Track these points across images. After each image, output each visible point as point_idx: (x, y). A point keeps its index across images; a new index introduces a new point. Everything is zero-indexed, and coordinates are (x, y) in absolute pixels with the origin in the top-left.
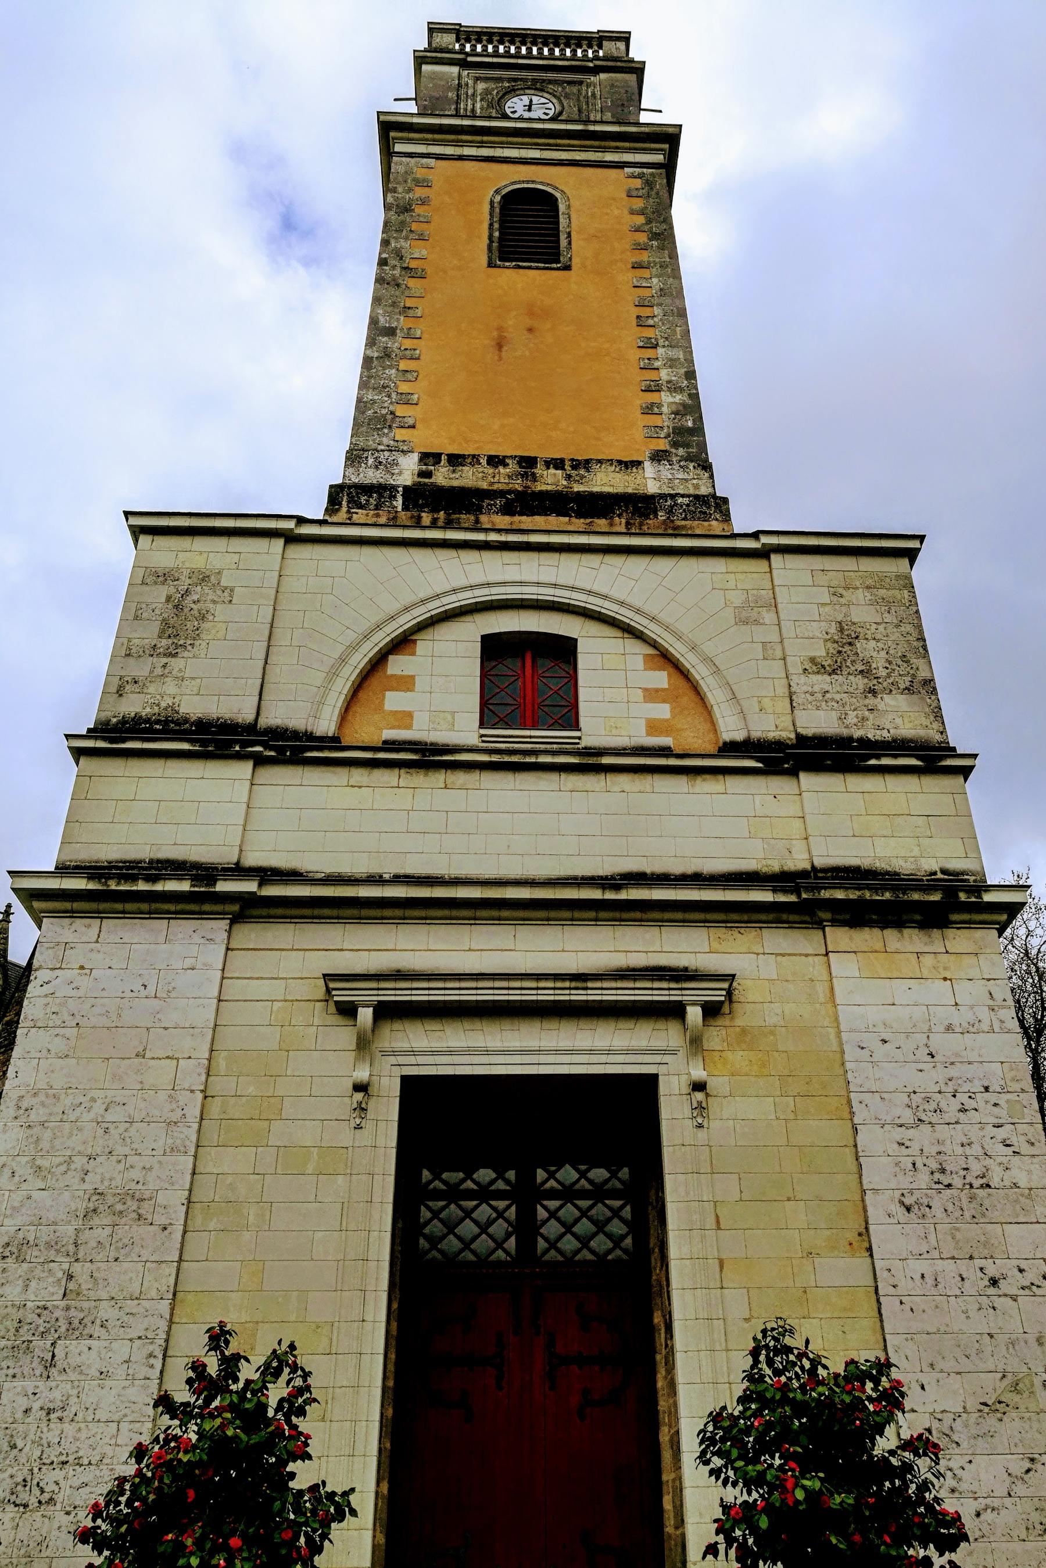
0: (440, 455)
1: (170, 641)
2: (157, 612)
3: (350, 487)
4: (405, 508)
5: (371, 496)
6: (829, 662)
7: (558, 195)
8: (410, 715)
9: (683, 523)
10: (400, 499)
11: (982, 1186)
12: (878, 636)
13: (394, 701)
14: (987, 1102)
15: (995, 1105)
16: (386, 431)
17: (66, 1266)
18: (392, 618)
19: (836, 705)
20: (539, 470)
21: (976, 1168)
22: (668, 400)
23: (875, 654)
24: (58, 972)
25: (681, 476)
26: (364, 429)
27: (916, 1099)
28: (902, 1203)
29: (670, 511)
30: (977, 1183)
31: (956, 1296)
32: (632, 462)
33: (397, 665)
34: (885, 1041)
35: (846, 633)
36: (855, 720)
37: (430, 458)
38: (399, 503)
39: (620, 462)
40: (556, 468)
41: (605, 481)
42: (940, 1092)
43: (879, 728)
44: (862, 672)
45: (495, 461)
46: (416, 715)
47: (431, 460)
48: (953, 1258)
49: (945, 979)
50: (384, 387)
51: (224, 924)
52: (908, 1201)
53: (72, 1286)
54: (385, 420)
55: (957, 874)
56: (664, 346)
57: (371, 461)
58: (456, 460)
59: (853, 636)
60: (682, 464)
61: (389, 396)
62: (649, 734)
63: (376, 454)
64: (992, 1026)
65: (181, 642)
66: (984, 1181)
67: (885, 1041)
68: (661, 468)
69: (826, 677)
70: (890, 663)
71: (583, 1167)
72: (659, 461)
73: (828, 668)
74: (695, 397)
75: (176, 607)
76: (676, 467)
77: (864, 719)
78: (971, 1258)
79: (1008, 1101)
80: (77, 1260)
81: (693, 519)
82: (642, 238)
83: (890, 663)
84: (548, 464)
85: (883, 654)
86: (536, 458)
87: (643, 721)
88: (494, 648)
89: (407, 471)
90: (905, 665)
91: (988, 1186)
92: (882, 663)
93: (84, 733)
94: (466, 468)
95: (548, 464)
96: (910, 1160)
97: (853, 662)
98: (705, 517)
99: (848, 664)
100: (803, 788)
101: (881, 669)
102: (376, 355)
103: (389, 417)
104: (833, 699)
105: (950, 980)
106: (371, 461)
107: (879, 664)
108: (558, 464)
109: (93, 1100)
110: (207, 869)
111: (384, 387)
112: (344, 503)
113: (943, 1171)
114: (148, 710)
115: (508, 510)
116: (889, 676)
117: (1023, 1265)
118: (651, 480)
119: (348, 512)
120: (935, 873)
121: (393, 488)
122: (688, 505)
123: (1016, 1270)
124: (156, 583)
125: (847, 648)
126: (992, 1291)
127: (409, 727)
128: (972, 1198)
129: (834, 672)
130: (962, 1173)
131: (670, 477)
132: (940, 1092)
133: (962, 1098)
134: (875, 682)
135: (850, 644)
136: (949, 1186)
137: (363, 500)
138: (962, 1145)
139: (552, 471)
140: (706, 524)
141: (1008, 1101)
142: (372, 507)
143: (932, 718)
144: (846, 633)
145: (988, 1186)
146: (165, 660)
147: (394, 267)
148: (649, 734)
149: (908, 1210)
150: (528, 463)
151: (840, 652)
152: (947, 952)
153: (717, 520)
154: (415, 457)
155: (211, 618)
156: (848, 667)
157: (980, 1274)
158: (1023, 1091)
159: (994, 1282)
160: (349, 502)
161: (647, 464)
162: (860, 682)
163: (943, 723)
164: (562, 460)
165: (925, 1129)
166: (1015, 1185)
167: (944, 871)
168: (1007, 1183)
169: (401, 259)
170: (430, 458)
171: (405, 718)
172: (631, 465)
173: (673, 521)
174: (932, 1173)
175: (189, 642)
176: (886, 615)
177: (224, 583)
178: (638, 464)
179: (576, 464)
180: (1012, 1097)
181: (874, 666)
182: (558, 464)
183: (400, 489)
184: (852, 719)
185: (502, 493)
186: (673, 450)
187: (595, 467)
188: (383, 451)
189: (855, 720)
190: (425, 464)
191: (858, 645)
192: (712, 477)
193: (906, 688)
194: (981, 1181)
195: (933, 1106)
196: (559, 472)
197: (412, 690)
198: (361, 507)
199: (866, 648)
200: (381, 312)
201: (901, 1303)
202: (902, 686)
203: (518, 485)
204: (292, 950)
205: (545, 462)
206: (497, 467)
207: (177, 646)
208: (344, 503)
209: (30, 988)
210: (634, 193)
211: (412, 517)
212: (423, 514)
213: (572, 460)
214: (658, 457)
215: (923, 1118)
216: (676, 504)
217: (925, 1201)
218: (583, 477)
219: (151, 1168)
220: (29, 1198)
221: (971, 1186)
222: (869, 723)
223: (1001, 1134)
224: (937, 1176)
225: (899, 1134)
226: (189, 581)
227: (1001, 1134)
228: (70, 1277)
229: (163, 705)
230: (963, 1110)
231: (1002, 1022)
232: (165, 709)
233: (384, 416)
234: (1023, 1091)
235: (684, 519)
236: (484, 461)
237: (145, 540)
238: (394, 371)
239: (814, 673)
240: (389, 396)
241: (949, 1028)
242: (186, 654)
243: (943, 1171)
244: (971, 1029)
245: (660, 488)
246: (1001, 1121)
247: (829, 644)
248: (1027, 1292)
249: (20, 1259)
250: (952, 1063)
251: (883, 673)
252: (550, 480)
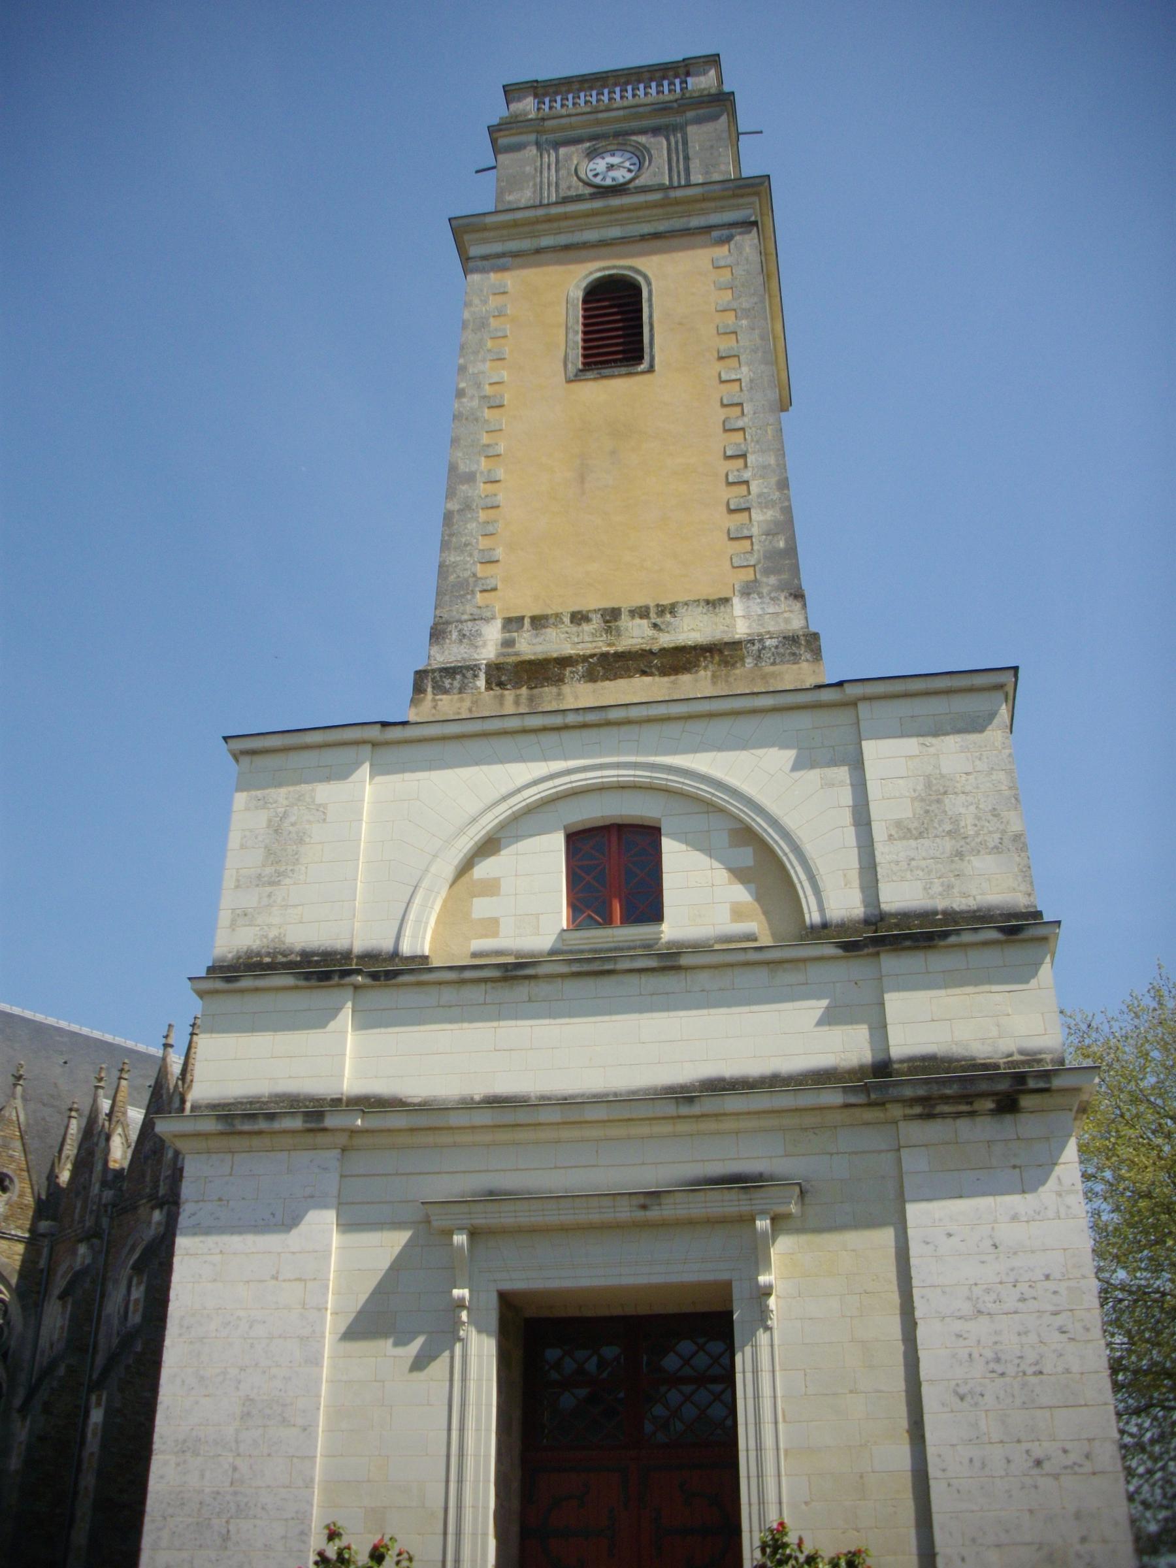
0: (523, 618)
1: (273, 868)
2: (260, 838)
3: (433, 671)
4: (489, 687)
5: (454, 679)
6: (916, 824)
7: (640, 279)
8: (495, 921)
9: (772, 668)
10: (482, 676)
11: (1035, 1374)
12: (968, 788)
13: (482, 907)
14: (1046, 1290)
15: (1055, 1292)
16: (469, 597)
17: (231, 1460)
18: (474, 820)
19: (921, 873)
20: (625, 622)
21: (1031, 1356)
22: (761, 517)
23: (963, 810)
24: (201, 1204)
25: (771, 610)
26: (447, 598)
27: (977, 1291)
28: (956, 1393)
29: (759, 657)
30: (1030, 1370)
31: (1001, 1477)
32: (720, 599)
33: (484, 869)
34: (949, 1235)
35: (934, 788)
36: (940, 889)
37: (512, 623)
38: (481, 683)
39: (708, 602)
40: (641, 618)
41: (691, 629)
42: (1001, 1283)
43: (965, 895)
44: (949, 833)
45: (579, 618)
46: (502, 920)
47: (514, 626)
48: (1001, 1442)
49: (1014, 1167)
50: (466, 545)
51: (336, 1153)
52: (962, 1390)
53: (237, 1476)
54: (468, 584)
55: (1035, 1053)
56: (754, 452)
57: (455, 635)
58: (539, 622)
59: (942, 790)
60: (773, 595)
61: (471, 555)
62: (734, 921)
63: (460, 626)
64: (1058, 1212)
65: (282, 869)
66: (1037, 1368)
67: (949, 1235)
68: (751, 603)
69: (913, 843)
70: (979, 819)
71: (701, 1341)
72: (748, 594)
73: (914, 832)
74: (788, 511)
75: (276, 831)
76: (767, 600)
77: (950, 887)
78: (1019, 1441)
79: (1068, 1288)
80: (239, 1455)
81: (782, 662)
82: (730, 318)
83: (979, 819)
84: (633, 613)
85: (972, 808)
86: (619, 609)
87: (728, 905)
88: (576, 840)
89: (489, 645)
90: (995, 819)
91: (1041, 1373)
92: (970, 821)
93: (203, 974)
94: (549, 630)
95: (633, 613)
96: (967, 1351)
97: (941, 822)
98: (795, 658)
99: (936, 825)
100: (884, 973)
101: (969, 828)
102: (456, 507)
103: (471, 580)
104: (918, 868)
105: (1020, 1167)
106: (455, 635)
107: (968, 825)
108: (642, 612)
109: (239, 1318)
110: (318, 1100)
111: (466, 545)
112: (429, 690)
113: (998, 1360)
114: (258, 942)
115: (591, 677)
116: (977, 834)
117: (1068, 1446)
118: (740, 621)
119: (434, 700)
120: (1011, 1055)
121: (474, 669)
122: (777, 647)
123: (1060, 1452)
124: (257, 808)
125: (934, 807)
126: (1035, 1471)
127: (495, 934)
128: (1024, 1385)
129: (920, 835)
130: (1017, 1361)
131: (760, 612)
132: (1001, 1283)
133: (1023, 1287)
134: (962, 843)
135: (938, 801)
136: (1003, 1374)
137: (447, 683)
138: (1019, 1334)
139: (638, 621)
140: (795, 667)
141: (1068, 1288)
142: (455, 691)
143: (1020, 879)
144: (934, 788)
145: (1041, 1373)
146: (268, 889)
147: (472, 398)
148: (734, 921)
149: (962, 1398)
150: (611, 616)
151: (927, 812)
152: (1018, 1139)
153: (807, 661)
154: (498, 623)
155: (307, 840)
156: (935, 828)
157: (1025, 1456)
158: (1084, 1277)
159: (1038, 1463)
160: (433, 688)
161: (736, 601)
162: (948, 845)
163: (1031, 883)
164: (647, 608)
165: (984, 1319)
166: (1068, 1371)
167: (1021, 1053)
168: (1060, 1369)
169: (479, 387)
170: (512, 623)
171: (491, 926)
172: (718, 603)
173: (761, 668)
174: (987, 1363)
175: (290, 868)
176: (978, 763)
177: (318, 801)
178: (726, 601)
179: (662, 610)
180: (1072, 1283)
181: (962, 824)
182: (642, 612)
183: (483, 667)
184: (937, 888)
185: (585, 658)
186: (765, 580)
187: (681, 610)
188: (466, 621)
189: (940, 889)
190: (509, 631)
191: (947, 801)
192: (804, 606)
193: (996, 847)
194: (1034, 1369)
195: (993, 1296)
196: (645, 622)
197: (498, 895)
198: (446, 692)
199: (955, 805)
200: (460, 454)
201: (949, 1485)
202: (991, 845)
203: (602, 646)
204: (397, 1174)
205: (630, 611)
206: (579, 625)
207: (279, 874)
208: (429, 690)
209: (181, 1219)
210: (722, 263)
211: (495, 697)
212: (506, 692)
213: (658, 605)
214: (748, 590)
215: (983, 1309)
216: (764, 648)
217: (979, 1389)
218: (669, 624)
219: (290, 1378)
220: (197, 1403)
221: (1024, 1373)
222: (955, 891)
223: (1059, 1320)
224: (992, 1366)
225: (958, 1326)
226: (285, 803)
227: (1059, 1320)
228: (235, 1469)
229: (271, 936)
230: (1023, 1300)
231: (1069, 1207)
232: (273, 941)
233: (466, 580)
234: (1084, 1277)
235: (774, 664)
236: (567, 620)
237: (245, 760)
238: (474, 525)
239: (900, 839)
240: (471, 555)
241: (1015, 1218)
242: (287, 881)
243: (998, 1360)
244: (1037, 1217)
245: (749, 627)
246: (1058, 1308)
247: (916, 804)
248: (1069, 1471)
249: (196, 1454)
250: (1015, 1253)
251: (971, 831)
252: (636, 634)
